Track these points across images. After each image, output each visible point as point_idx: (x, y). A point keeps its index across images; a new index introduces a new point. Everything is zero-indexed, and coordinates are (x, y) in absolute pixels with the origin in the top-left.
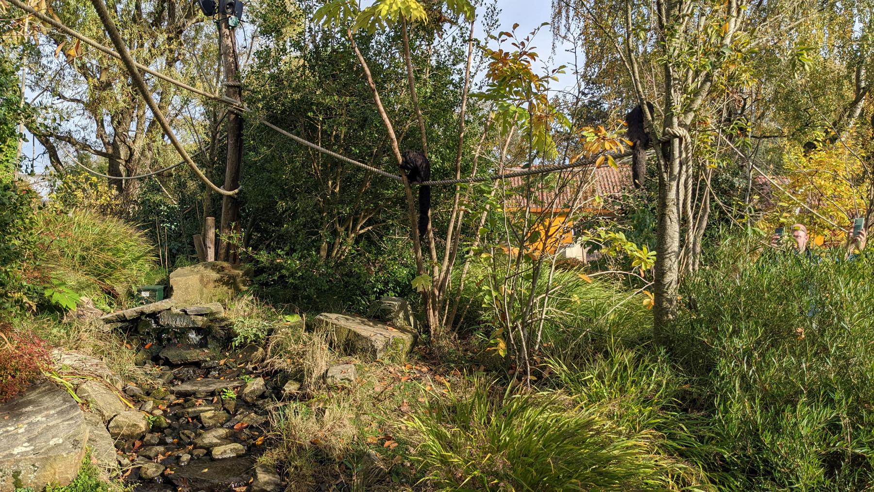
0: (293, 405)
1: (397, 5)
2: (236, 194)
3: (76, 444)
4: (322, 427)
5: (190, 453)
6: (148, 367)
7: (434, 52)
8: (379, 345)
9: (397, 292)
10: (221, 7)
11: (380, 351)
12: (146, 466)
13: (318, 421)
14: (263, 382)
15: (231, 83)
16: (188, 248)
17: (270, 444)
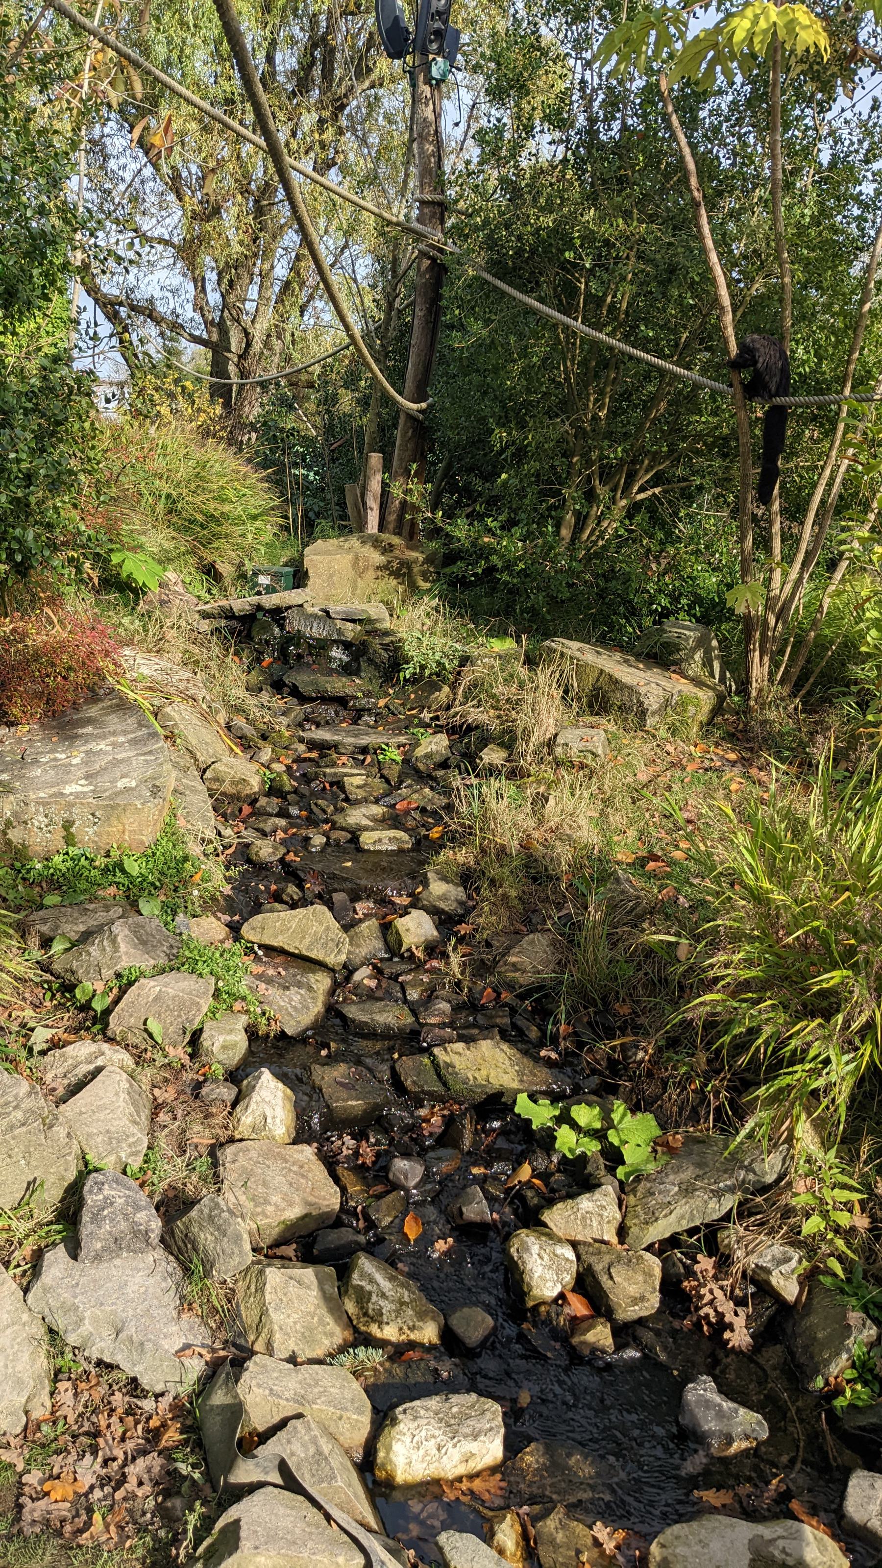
0: (495, 784)
1: (767, 19)
2: (421, 411)
3: (155, 791)
4: (540, 823)
5: (326, 834)
6: (265, 696)
7: (830, 134)
8: (652, 703)
9: (694, 616)
10: (419, 43)
11: (654, 714)
12: (258, 843)
13: (534, 812)
14: (446, 743)
15: (428, 197)
16: (335, 510)
17: (453, 839)
